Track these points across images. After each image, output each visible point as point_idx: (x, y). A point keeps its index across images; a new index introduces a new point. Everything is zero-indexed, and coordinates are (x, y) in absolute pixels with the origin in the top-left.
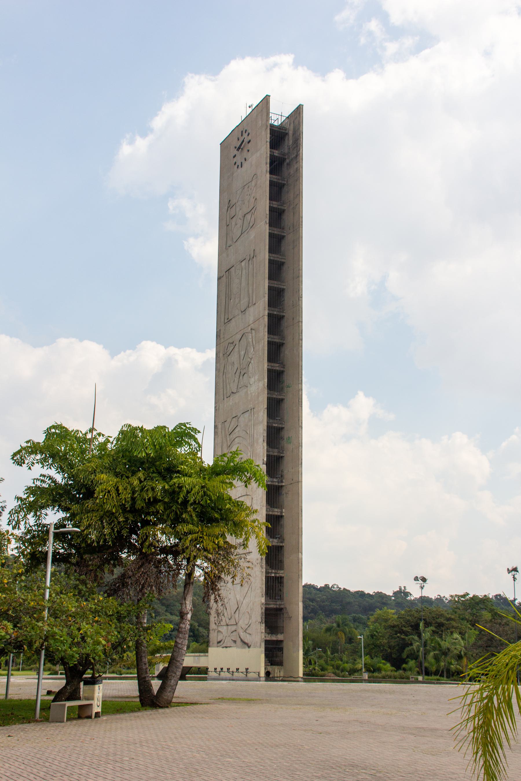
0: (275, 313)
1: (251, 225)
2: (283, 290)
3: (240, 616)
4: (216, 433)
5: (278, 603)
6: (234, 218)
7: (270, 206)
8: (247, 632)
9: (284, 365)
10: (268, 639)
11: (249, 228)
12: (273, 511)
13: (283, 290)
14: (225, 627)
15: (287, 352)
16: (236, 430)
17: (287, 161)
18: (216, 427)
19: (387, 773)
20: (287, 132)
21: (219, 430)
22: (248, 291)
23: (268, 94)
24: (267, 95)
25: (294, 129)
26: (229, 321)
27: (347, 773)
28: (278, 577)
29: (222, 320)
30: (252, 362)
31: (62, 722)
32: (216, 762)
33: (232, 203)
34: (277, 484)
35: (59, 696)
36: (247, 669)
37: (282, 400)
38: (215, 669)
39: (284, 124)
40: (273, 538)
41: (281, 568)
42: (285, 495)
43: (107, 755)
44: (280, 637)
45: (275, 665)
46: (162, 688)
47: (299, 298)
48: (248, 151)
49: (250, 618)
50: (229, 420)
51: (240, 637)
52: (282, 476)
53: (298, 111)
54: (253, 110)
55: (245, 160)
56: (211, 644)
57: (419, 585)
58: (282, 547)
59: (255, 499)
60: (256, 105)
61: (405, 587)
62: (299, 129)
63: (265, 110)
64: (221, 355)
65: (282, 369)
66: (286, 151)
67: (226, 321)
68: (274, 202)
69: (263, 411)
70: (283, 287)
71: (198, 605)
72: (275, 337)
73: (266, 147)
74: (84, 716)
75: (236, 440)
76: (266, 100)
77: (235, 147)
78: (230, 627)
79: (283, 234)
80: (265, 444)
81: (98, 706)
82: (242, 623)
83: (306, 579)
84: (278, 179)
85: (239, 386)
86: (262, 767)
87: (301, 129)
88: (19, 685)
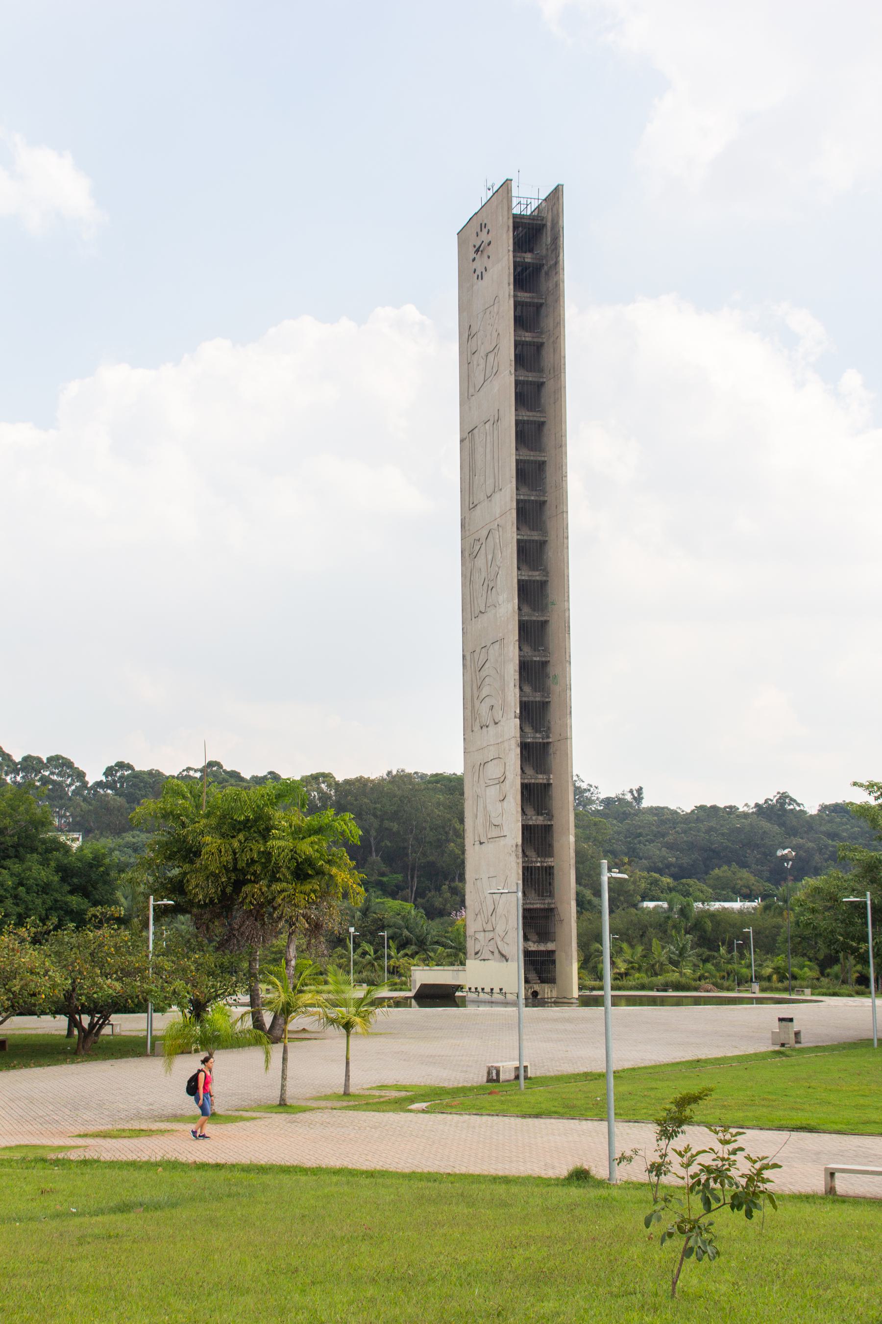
0: (533, 498)
2: (544, 462)
5: (546, 901)
9: (548, 573)
12: (536, 779)
13: (544, 462)
14: (482, 934)
15: (550, 554)
17: (546, 268)
18: (464, 656)
20: (544, 222)
21: (468, 663)
23: (510, 178)
25: (553, 220)
34: (541, 740)
37: (546, 622)
44: (550, 946)
47: (563, 477)
48: (489, 257)
50: (478, 650)
53: (556, 194)
59: (507, 764)
62: (558, 222)
63: (505, 201)
65: (544, 578)
66: (544, 252)
70: (543, 459)
71: (592, 857)
72: (533, 533)
73: (508, 260)
75: (487, 679)
76: (507, 183)
77: (473, 244)
78: (487, 933)
82: (500, 929)
84: (533, 298)
87: (561, 222)
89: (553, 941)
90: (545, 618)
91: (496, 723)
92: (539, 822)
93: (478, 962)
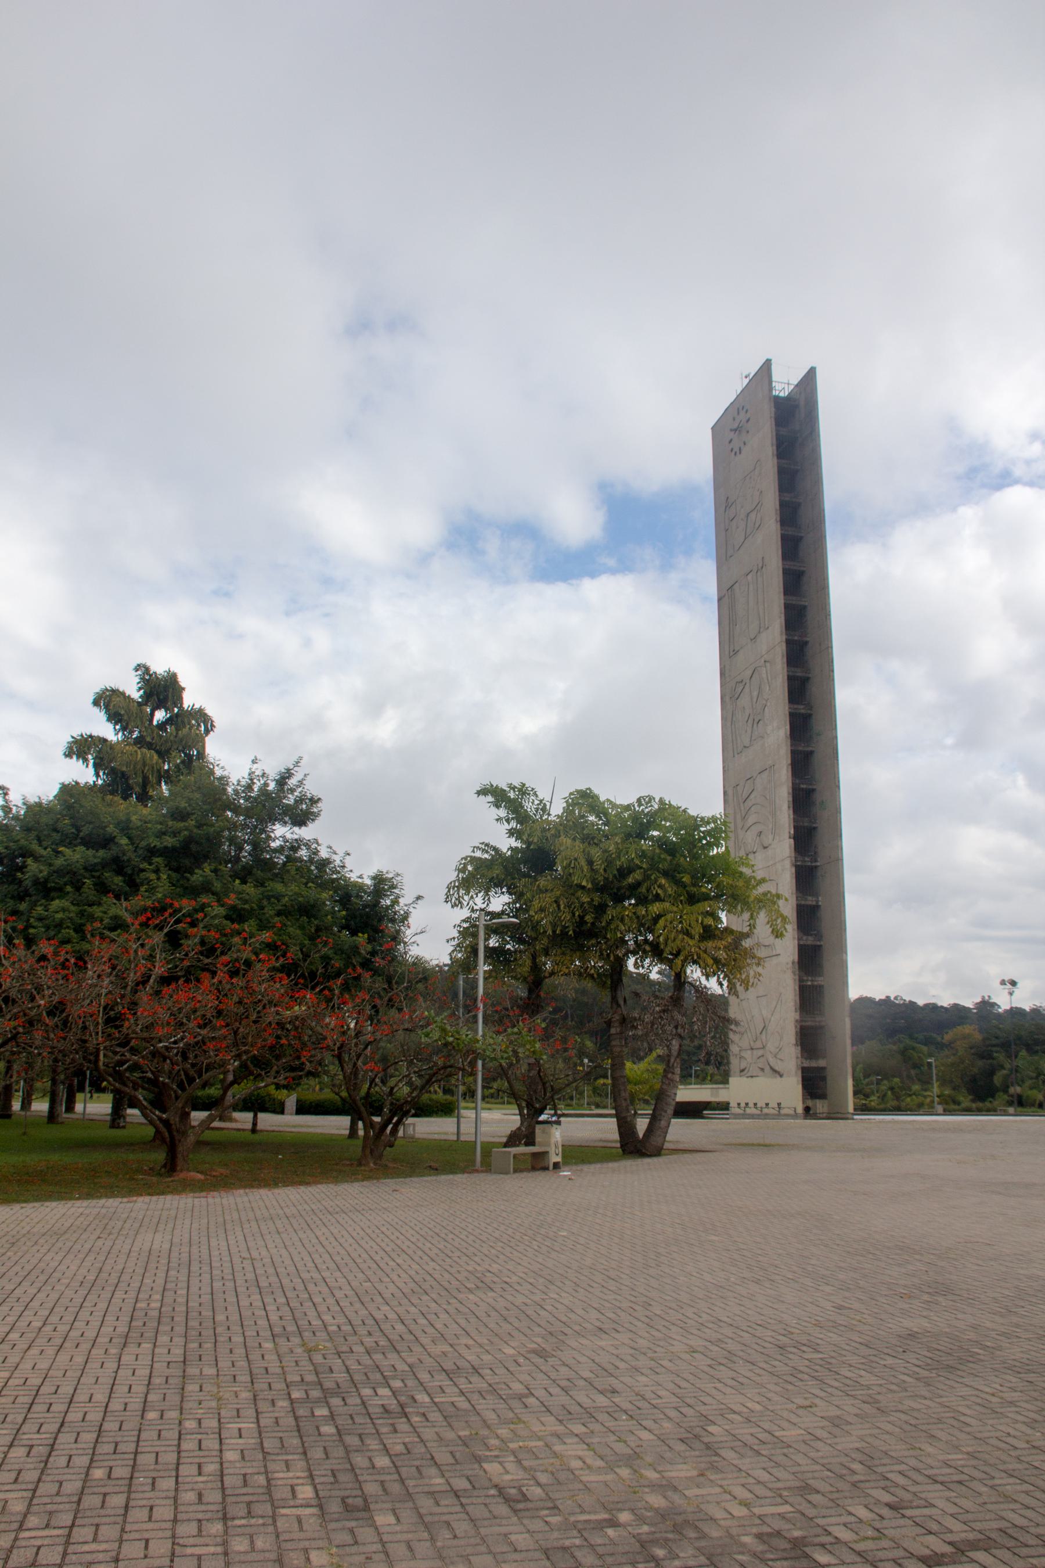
2: (805, 607)
4: (725, 801)
10: (805, 1065)
13: (805, 607)
14: (749, 1052)
16: (752, 796)
18: (725, 793)
26: (736, 652)
29: (727, 653)
31: (507, 1173)
35: (513, 1139)
36: (779, 1104)
37: (812, 752)
38: (739, 1104)
44: (821, 1063)
46: (650, 1130)
53: (811, 375)
56: (732, 1073)
58: (820, 946)
64: (727, 699)
76: (767, 365)
77: (729, 433)
78: (755, 1052)
80: (791, 812)
82: (771, 1046)
88: (133, 1115)
89: (824, 1057)
90: (810, 749)
91: (765, 848)
92: (809, 943)
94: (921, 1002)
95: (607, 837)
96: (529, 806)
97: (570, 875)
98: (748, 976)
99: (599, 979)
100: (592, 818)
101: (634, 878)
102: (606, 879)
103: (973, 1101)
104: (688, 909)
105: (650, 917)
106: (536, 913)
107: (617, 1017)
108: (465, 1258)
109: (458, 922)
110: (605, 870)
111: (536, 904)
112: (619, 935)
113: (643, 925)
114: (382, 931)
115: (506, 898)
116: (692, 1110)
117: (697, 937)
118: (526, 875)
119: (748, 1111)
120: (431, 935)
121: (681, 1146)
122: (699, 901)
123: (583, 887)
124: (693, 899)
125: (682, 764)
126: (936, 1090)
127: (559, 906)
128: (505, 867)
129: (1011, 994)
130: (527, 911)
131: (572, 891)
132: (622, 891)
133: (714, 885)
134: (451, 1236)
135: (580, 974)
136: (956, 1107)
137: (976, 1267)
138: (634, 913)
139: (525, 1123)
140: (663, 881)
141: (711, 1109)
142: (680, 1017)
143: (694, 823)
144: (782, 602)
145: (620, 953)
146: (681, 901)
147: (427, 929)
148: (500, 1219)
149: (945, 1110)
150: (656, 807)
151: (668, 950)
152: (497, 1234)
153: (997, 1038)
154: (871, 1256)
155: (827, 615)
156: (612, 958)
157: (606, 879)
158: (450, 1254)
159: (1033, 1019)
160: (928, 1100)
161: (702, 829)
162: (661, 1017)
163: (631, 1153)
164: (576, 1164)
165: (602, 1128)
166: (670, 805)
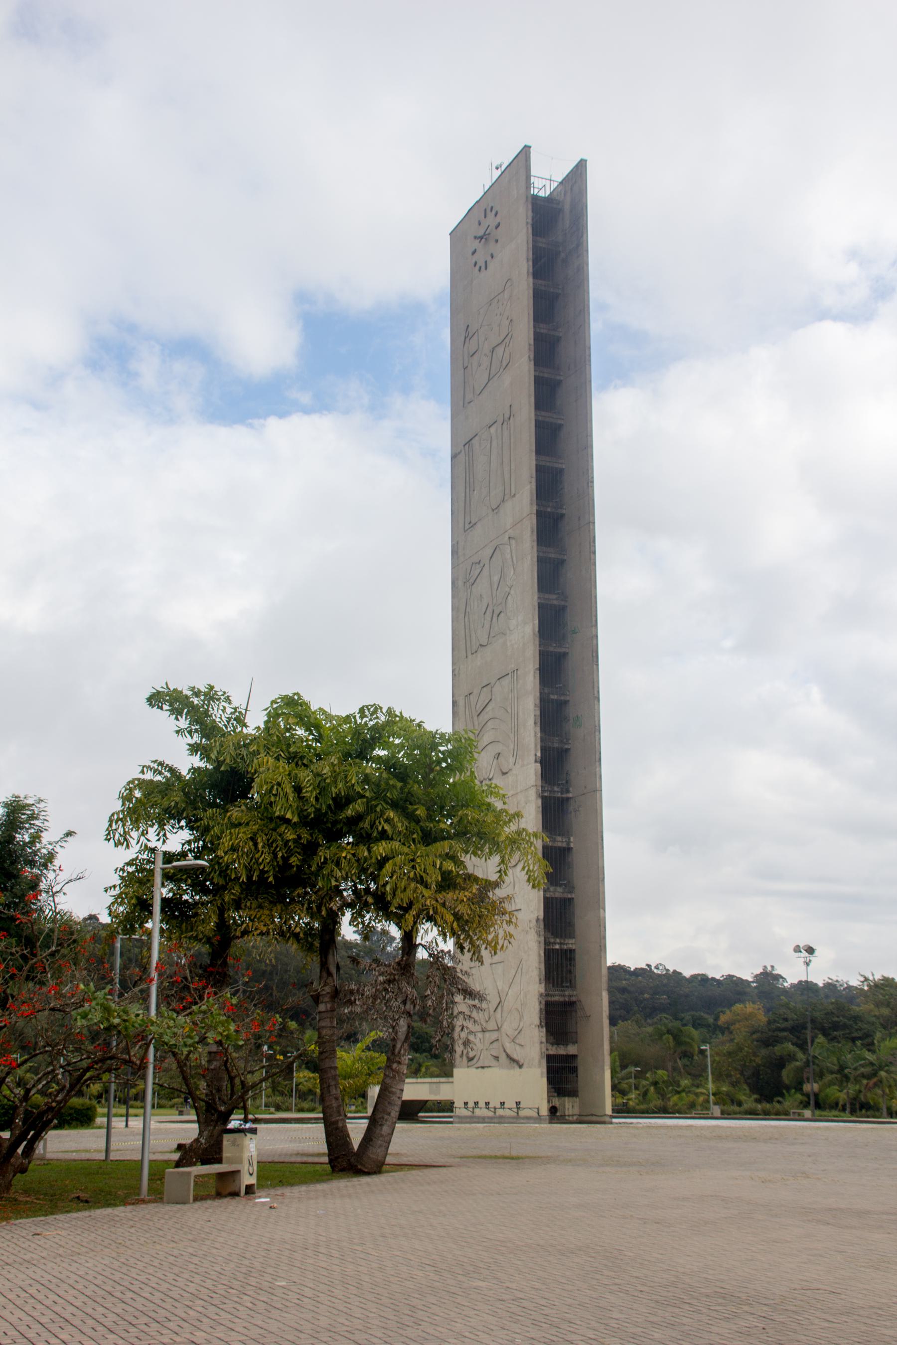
0: (549, 510)
1: (504, 364)
3: (505, 1015)
4: (455, 714)
5: (567, 993)
6: (475, 356)
7: (534, 332)
8: (517, 1041)
10: (551, 1052)
11: (502, 370)
17: (563, 255)
18: (454, 703)
19: (795, 1312)
22: (503, 473)
23: (528, 144)
24: (525, 146)
26: (473, 525)
27: (714, 1314)
28: (566, 950)
29: (461, 525)
30: (512, 592)
32: (453, 1289)
33: (472, 330)
34: (559, 795)
35: (188, 1154)
36: (518, 1103)
38: (466, 1104)
39: (555, 194)
40: (556, 885)
41: (571, 936)
42: (573, 813)
43: (248, 1274)
44: (572, 1050)
45: (565, 1096)
46: (368, 1138)
48: (497, 241)
49: (521, 1018)
50: (476, 692)
51: (505, 1051)
52: (567, 782)
53: (579, 172)
54: (502, 173)
55: (492, 257)
57: (803, 960)
58: (571, 900)
60: (508, 164)
61: (772, 967)
64: (460, 583)
65: (563, 603)
67: (467, 526)
68: (541, 325)
69: (532, 673)
70: (560, 466)
74: (227, 1192)
75: (489, 724)
76: (525, 153)
77: (474, 238)
78: (487, 1035)
79: (558, 378)
80: (538, 729)
81: (251, 1175)
82: (508, 1028)
83: (613, 958)
85: (492, 634)
86: (543, 1302)
90: (563, 650)
91: (504, 774)
92: (557, 895)
93: (473, 1070)
94: (687, 973)
95: (318, 756)
96: (219, 714)
97: (271, 804)
98: (497, 936)
99: (305, 939)
100: (300, 732)
101: (354, 809)
102: (318, 810)
103: (758, 1101)
104: (422, 849)
105: (373, 860)
106: (226, 853)
107: (328, 989)
108: (155, 1325)
109: (121, 866)
110: (317, 799)
111: (226, 842)
112: (334, 883)
113: (363, 870)
114: (16, 877)
115: (186, 835)
116: (411, 1111)
117: (433, 886)
118: (214, 805)
119: (478, 1112)
120: (83, 881)
121: (404, 1160)
122: (436, 840)
123: (288, 821)
124: (429, 838)
125: (399, 665)
126: (711, 1086)
127: (256, 845)
128: (186, 795)
129: (807, 964)
130: (213, 850)
131: (272, 826)
132: (339, 826)
133: (456, 820)
134: (130, 1294)
135: (282, 934)
136: (736, 1108)
137: (826, 1324)
138: (354, 855)
139: (206, 1133)
140: (392, 814)
141: (426, 1112)
142: (410, 989)
143: (430, 741)
144: (534, 463)
145: (334, 906)
146: (414, 840)
147: (86, 874)
148: (192, 1267)
149: (722, 1113)
150: (383, 718)
151: (396, 902)
152: (192, 1288)
153: (786, 1020)
154: (687, 1307)
155: (590, 482)
156: (324, 913)
157: (319, 810)
158: (135, 1322)
159: (827, 997)
160: (701, 1099)
161: (442, 749)
162: (386, 990)
163: (343, 1170)
164: (273, 1186)
165: (306, 1137)
166: (401, 717)
